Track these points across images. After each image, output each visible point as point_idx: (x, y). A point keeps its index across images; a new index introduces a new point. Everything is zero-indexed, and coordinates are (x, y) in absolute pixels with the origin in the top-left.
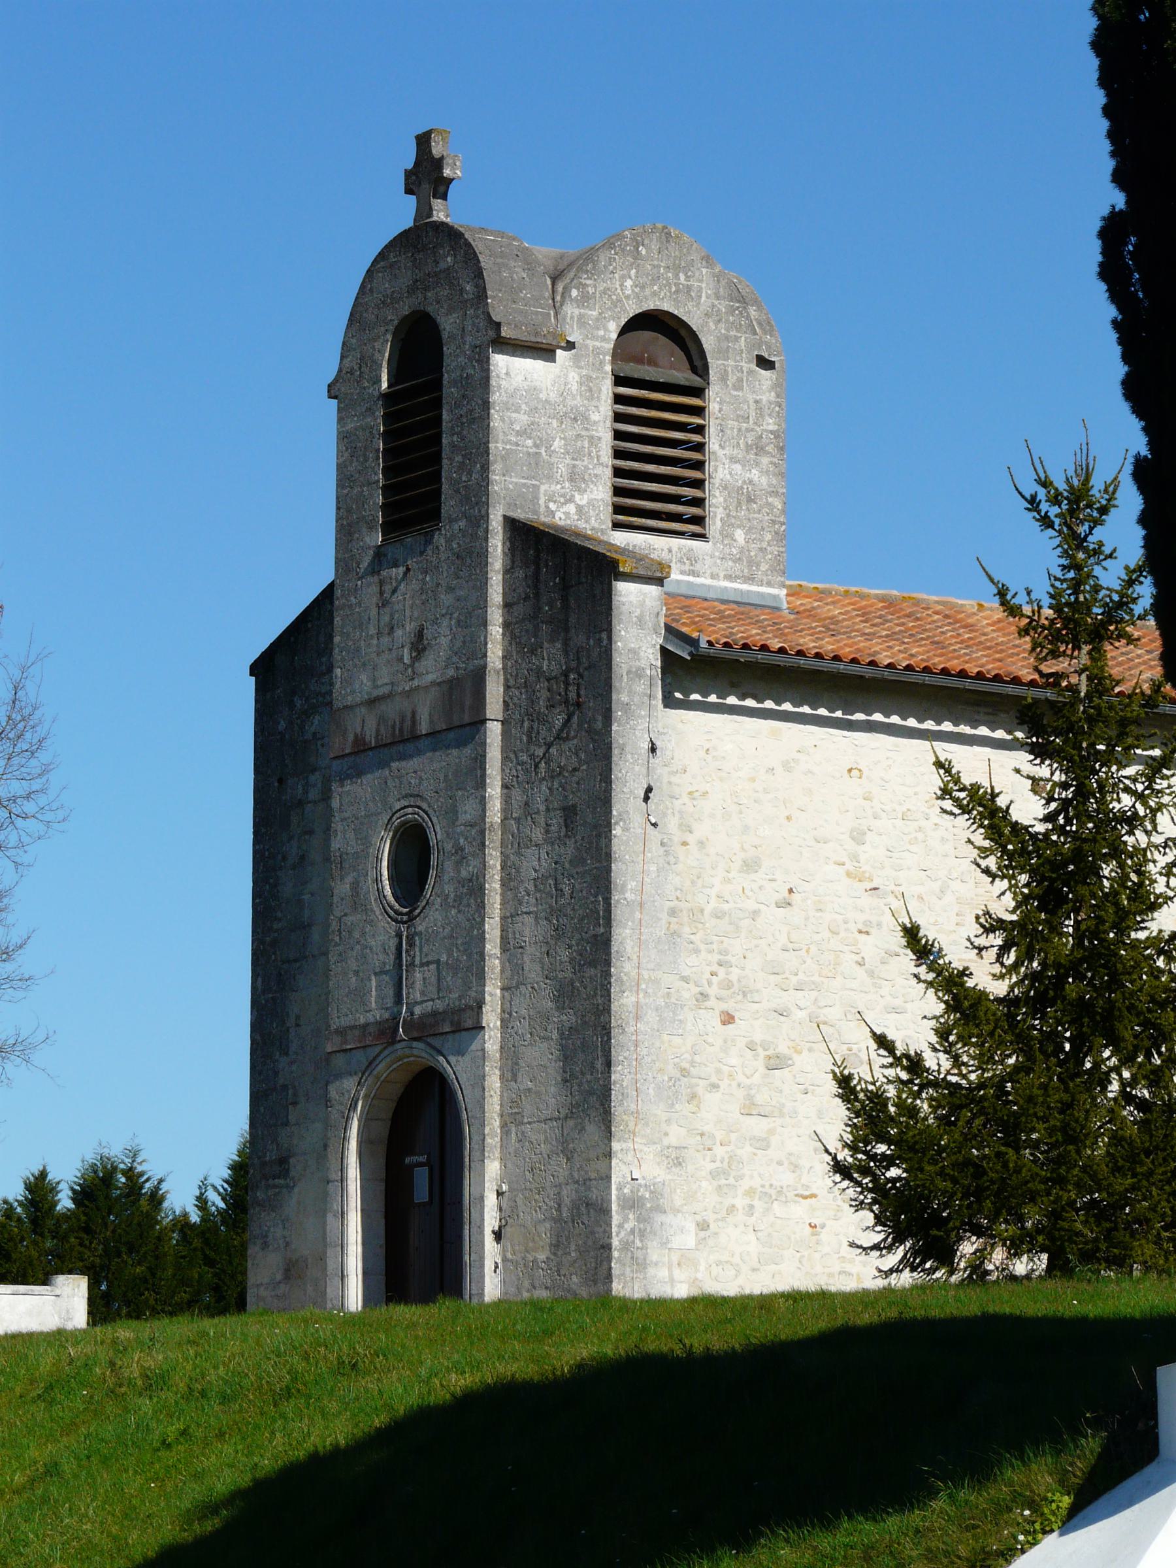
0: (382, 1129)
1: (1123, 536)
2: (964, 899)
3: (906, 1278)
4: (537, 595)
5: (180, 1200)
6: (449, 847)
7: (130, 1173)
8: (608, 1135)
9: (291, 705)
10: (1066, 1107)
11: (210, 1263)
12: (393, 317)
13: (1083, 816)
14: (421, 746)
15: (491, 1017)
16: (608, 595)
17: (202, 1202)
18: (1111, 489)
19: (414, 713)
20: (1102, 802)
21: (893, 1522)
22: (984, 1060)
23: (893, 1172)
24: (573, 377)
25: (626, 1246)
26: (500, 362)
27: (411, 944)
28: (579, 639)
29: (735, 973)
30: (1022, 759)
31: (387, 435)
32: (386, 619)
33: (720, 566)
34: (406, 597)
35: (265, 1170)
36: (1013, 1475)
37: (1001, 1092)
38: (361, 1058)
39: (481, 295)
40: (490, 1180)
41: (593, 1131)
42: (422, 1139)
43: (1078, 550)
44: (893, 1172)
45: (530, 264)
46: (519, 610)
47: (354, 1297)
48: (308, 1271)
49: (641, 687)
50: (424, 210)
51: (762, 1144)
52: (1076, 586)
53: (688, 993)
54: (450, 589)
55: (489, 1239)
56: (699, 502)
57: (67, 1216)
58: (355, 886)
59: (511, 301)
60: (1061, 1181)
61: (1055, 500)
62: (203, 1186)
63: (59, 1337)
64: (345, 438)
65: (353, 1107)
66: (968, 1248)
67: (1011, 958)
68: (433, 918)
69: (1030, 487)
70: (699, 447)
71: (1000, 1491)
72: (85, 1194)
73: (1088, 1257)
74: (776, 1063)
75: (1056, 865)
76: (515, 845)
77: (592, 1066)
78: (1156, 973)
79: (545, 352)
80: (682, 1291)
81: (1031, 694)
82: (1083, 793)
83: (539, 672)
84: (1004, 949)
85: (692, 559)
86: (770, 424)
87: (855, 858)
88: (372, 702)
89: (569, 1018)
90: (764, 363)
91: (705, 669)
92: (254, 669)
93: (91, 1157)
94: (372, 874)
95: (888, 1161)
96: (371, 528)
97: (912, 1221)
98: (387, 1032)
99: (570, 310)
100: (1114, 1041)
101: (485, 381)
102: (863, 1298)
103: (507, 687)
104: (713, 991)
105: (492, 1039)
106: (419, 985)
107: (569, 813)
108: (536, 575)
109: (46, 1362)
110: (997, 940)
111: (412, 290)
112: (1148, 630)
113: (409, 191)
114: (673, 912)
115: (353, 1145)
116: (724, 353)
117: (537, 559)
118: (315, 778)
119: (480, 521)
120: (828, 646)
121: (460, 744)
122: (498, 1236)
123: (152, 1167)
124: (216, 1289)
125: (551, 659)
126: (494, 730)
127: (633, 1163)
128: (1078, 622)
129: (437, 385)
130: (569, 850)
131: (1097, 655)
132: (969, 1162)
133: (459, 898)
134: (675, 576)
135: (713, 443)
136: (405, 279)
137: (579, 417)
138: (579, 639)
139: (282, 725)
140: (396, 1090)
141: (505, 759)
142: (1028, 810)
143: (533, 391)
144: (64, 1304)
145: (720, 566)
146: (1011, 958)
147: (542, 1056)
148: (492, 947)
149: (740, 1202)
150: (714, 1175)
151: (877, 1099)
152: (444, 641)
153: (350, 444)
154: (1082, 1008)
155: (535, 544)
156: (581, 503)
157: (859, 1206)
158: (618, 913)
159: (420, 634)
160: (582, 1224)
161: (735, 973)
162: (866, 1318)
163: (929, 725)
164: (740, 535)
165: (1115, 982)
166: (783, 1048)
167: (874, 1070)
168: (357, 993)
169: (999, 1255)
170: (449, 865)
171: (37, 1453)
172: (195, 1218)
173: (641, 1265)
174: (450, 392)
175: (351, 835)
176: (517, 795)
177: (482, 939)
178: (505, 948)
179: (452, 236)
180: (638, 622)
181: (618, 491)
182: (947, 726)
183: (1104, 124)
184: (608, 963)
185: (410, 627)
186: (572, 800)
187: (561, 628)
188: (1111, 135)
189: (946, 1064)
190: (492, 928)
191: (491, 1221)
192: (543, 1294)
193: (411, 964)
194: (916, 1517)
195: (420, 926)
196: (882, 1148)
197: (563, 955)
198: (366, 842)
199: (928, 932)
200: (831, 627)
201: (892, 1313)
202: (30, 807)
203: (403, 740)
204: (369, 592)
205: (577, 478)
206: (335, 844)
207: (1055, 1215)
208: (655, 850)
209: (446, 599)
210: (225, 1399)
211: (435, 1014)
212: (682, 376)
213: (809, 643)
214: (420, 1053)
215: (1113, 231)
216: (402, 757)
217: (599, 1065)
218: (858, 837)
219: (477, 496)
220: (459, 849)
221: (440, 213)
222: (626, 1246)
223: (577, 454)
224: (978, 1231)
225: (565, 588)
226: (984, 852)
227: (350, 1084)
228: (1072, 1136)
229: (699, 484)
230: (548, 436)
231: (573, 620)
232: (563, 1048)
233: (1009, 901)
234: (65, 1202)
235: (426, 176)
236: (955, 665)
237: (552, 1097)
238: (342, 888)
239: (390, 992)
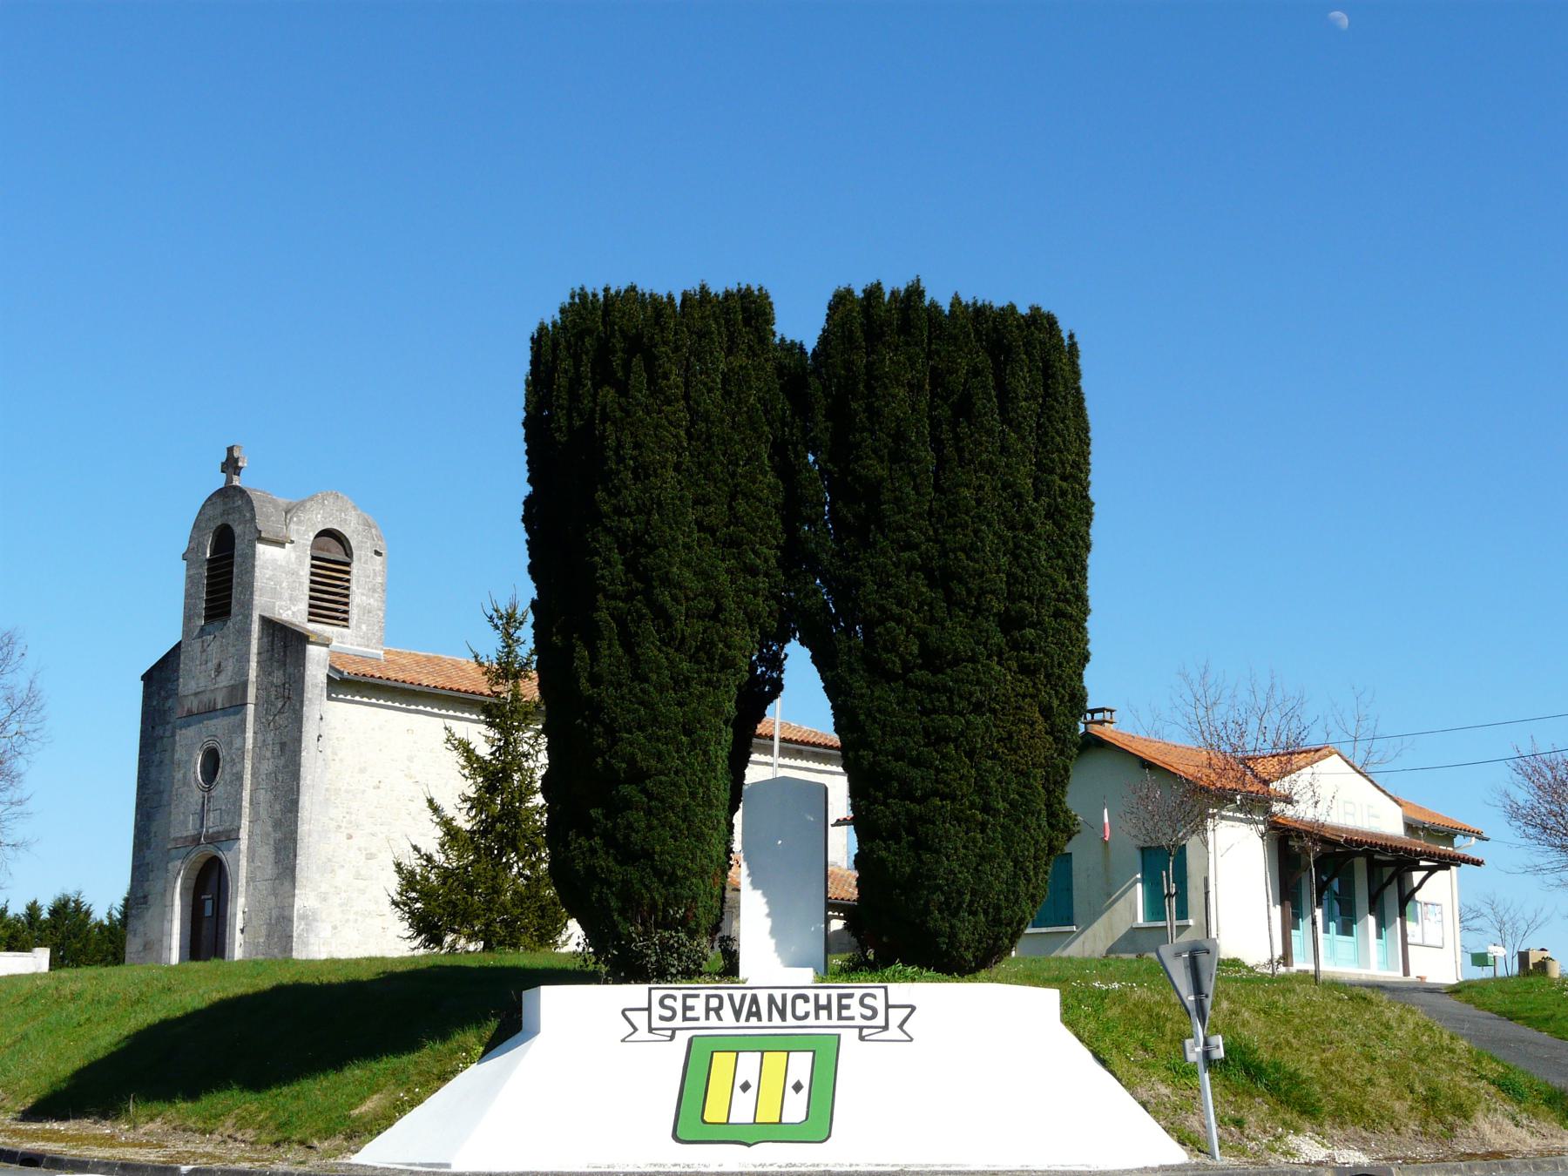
0: (192, 883)
1: (526, 634)
2: (454, 788)
3: (422, 951)
5: (100, 914)
7: (76, 902)
8: (294, 887)
10: (494, 878)
11: (112, 942)
12: (213, 526)
13: (506, 753)
14: (217, 707)
15: (244, 835)
16: (304, 650)
17: (110, 915)
18: (524, 615)
20: (515, 748)
21: (405, 1059)
22: (460, 857)
23: (418, 905)
24: (293, 556)
25: (299, 936)
28: (290, 670)
29: (353, 818)
30: (483, 728)
33: (353, 641)
34: (214, 648)
35: (137, 901)
36: (459, 1038)
37: (466, 869)
38: (183, 851)
39: (253, 518)
40: (240, 907)
41: (287, 884)
42: (210, 886)
43: (509, 640)
44: (418, 905)
45: (276, 505)
46: (265, 656)
47: (175, 958)
48: (153, 947)
49: (317, 691)
50: (229, 480)
51: (363, 892)
52: (508, 655)
53: (333, 824)
56: (346, 612)
57: (45, 921)
59: (266, 521)
60: (490, 910)
61: (501, 618)
62: (111, 908)
63: (34, 976)
66: (449, 939)
67: (473, 813)
68: (219, 790)
69: (490, 612)
70: (347, 588)
71: (453, 1044)
72: (55, 912)
73: (500, 943)
74: (370, 856)
75: (495, 774)
76: (258, 759)
78: (535, 822)
79: (281, 544)
80: (323, 957)
81: (489, 700)
82: (507, 743)
83: (272, 684)
84: (471, 808)
85: (342, 636)
86: (379, 580)
88: (196, 694)
89: (279, 835)
90: (377, 553)
91: (343, 684)
92: (143, 678)
93: (59, 895)
95: (417, 900)
97: (427, 927)
98: (196, 840)
99: (293, 527)
100: (516, 849)
101: (253, 556)
102: (402, 960)
105: (244, 843)
107: (283, 745)
109: (26, 988)
110: (468, 805)
111: (222, 515)
112: (534, 674)
115: (178, 890)
116: (360, 548)
118: (169, 727)
119: (248, 616)
120: (401, 676)
121: (236, 713)
122: (242, 931)
123: (86, 900)
124: (114, 954)
125: (278, 677)
126: (251, 708)
127: (304, 899)
128: (507, 671)
129: (232, 556)
130: (282, 762)
131: (516, 686)
132: (450, 901)
134: (334, 643)
135: (354, 586)
136: (219, 510)
137: (294, 573)
138: (290, 670)
140: (199, 866)
142: (484, 751)
143: (275, 561)
144: (38, 961)
145: (353, 641)
146: (473, 813)
147: (266, 852)
148: (246, 803)
151: (412, 873)
153: (190, 579)
154: (502, 835)
155: (270, 625)
156: (294, 610)
157: (402, 919)
158: (302, 789)
160: (280, 926)
161: (353, 818)
162: (400, 969)
163: (443, 712)
164: (364, 627)
165: (518, 824)
166: (373, 850)
167: (412, 862)
168: (182, 822)
169: (462, 941)
170: (228, 768)
171: (18, 1030)
172: (106, 922)
173: (306, 944)
174: (237, 559)
177: (241, 799)
179: (241, 492)
180: (317, 664)
181: (311, 606)
182: (451, 713)
183: (526, 458)
185: (215, 662)
188: (528, 462)
189: (443, 858)
190: (246, 795)
191: (239, 924)
192: (261, 957)
194: (415, 1057)
195: (213, 793)
196: (414, 895)
197: (277, 807)
198: (191, 756)
199: (438, 801)
200: (403, 669)
201: (412, 967)
202: (35, 736)
203: (210, 711)
204: (197, 645)
205: (292, 599)
206: (177, 756)
207: (487, 925)
208: (320, 763)
210: (108, 1004)
212: (341, 557)
213: (392, 675)
214: (211, 850)
215: (528, 503)
218: (410, 759)
219: (248, 605)
221: (236, 482)
222: (299, 936)
223: (293, 589)
224: (454, 931)
225: (285, 647)
226: (464, 767)
227: (178, 863)
228: (496, 890)
229: (346, 604)
230: (279, 579)
233: (473, 789)
234: (45, 915)
235: (231, 465)
236: (455, 687)
237: (270, 870)
238: (179, 776)
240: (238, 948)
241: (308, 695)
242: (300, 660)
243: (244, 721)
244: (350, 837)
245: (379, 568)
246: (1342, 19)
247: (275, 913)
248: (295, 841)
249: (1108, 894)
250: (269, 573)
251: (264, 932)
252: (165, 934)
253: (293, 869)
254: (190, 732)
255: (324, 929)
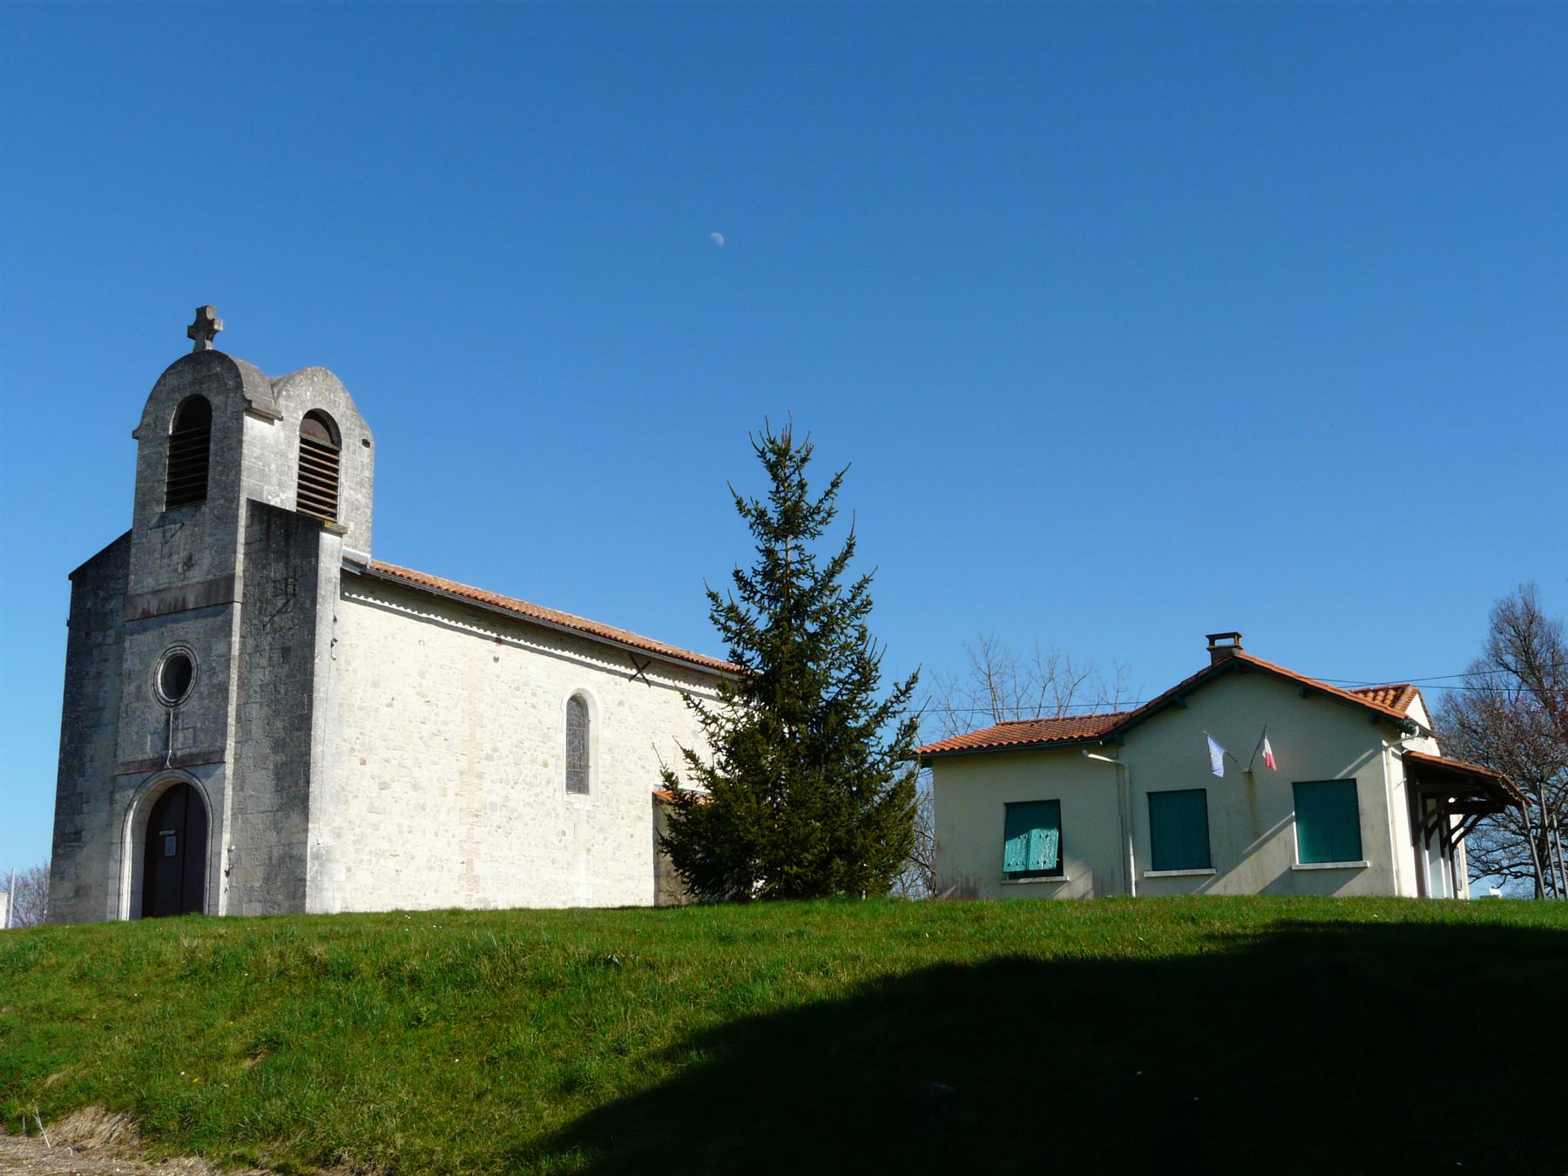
0: (146, 817)
4: (268, 539)
6: (205, 667)
9: (96, 594)
12: (179, 398)
15: (229, 757)
19: (345, 560)
24: (282, 434)
25: (314, 879)
26: (249, 421)
27: (176, 717)
29: (367, 739)
31: (171, 457)
32: (166, 549)
38: (138, 778)
40: (224, 845)
46: (256, 546)
47: (125, 915)
51: (376, 827)
53: (346, 747)
54: (211, 534)
55: (223, 874)
58: (139, 688)
59: (255, 387)
64: (143, 459)
65: (130, 806)
68: (192, 703)
74: (384, 786)
76: (248, 667)
77: (297, 784)
83: (268, 579)
87: (420, 685)
88: (155, 592)
89: (282, 758)
90: (366, 443)
94: (150, 682)
96: (159, 503)
98: (158, 764)
99: (282, 401)
103: (246, 585)
104: (357, 747)
105: (229, 768)
106: (181, 739)
107: (286, 652)
108: (268, 528)
111: (191, 384)
113: (190, 336)
114: (341, 705)
116: (349, 435)
117: (269, 521)
118: (112, 632)
122: (227, 873)
126: (237, 607)
127: (319, 835)
129: (208, 431)
133: (210, 694)
139: (89, 605)
140: (158, 795)
141: (243, 622)
143: (263, 438)
147: (262, 779)
148: (231, 720)
149: (366, 858)
150: (355, 843)
152: (207, 561)
153: (146, 464)
155: (260, 510)
158: (316, 703)
159: (190, 558)
160: (287, 870)
161: (367, 739)
163: (453, 623)
166: (387, 779)
174: (215, 434)
175: (137, 661)
176: (250, 642)
178: (238, 719)
181: (300, 495)
182: (460, 625)
184: (310, 729)
186: (288, 644)
187: (284, 555)
191: (224, 866)
193: (176, 729)
195: (183, 708)
197: (279, 724)
198: (148, 666)
203: (177, 611)
204: (156, 537)
209: (208, 540)
211: (191, 755)
212: (328, 444)
214: (181, 776)
216: (176, 621)
217: (301, 783)
218: (422, 675)
219: (233, 487)
220: (212, 669)
222: (314, 879)
225: (287, 536)
227: (131, 792)
230: (268, 462)
231: (292, 551)
232: (277, 774)
235: (202, 327)
237: (268, 799)
239: (160, 744)
240: (222, 897)
241: (321, 591)
242: (311, 551)
243: (229, 622)
244: (363, 762)
245: (367, 460)
246: (720, 239)
247: (276, 852)
248: (307, 765)
249: (1255, 833)
250: (257, 452)
251: (260, 873)
252: (108, 880)
253: (305, 799)
254: (148, 638)
255: (338, 872)
